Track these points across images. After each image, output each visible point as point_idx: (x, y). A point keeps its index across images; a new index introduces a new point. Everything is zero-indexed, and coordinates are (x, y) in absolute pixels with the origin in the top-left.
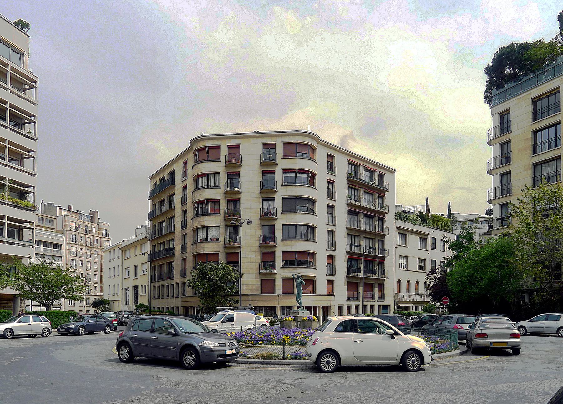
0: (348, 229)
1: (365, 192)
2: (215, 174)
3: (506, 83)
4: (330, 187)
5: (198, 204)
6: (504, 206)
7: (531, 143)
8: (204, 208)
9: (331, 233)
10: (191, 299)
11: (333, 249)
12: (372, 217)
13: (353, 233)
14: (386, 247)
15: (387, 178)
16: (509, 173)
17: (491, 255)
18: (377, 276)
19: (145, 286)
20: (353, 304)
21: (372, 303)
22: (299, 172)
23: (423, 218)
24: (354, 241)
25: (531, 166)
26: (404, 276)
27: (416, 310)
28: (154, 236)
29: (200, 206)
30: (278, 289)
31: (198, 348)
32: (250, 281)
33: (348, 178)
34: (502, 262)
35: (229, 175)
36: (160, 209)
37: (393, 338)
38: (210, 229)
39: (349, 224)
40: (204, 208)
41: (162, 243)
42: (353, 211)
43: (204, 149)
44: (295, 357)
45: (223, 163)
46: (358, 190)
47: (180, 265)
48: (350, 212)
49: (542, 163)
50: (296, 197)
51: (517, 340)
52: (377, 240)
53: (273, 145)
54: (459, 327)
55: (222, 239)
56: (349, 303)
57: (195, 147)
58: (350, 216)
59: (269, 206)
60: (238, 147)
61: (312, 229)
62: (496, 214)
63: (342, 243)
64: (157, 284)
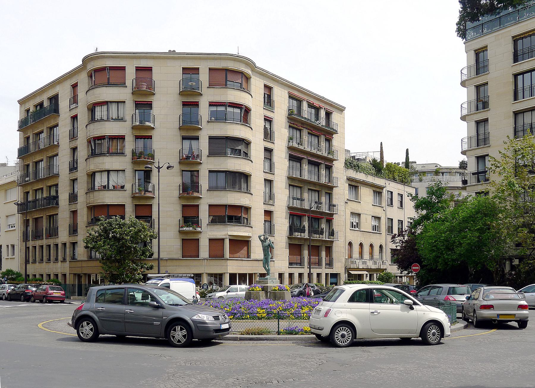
0: (290, 178)
1: (309, 133)
2: (118, 102)
3: (483, 15)
4: (268, 126)
5: (95, 141)
6: (481, 159)
7: (512, 88)
8: (99, 145)
9: (269, 182)
10: (84, 264)
11: (271, 202)
12: (317, 165)
13: (295, 183)
14: (334, 202)
15: (335, 117)
16: (486, 121)
17: (470, 217)
18: (325, 237)
19: (13, 246)
20: (296, 271)
21: (319, 271)
22: (229, 106)
23: (378, 167)
24: (297, 193)
25: (512, 114)
26: (356, 238)
27: (370, 280)
28: (27, 179)
29: (97, 142)
30: (204, 251)
31: (190, 321)
32: (167, 239)
33: (289, 115)
34: (483, 225)
35: (138, 105)
36: (36, 143)
37: (412, 308)
38: (111, 173)
39: (291, 171)
40: (99, 145)
41: (39, 189)
42: (295, 156)
43: (103, 69)
44: (291, 332)
46: (300, 130)
47: (68, 219)
48: (292, 158)
49: (523, 112)
50: (227, 137)
51: (525, 312)
52: (324, 193)
53: (196, 70)
54: (451, 299)
55: (128, 187)
56: (292, 271)
57: (91, 66)
58: (291, 162)
59: (191, 148)
60: (150, 69)
61: (246, 177)
62: (472, 167)
63: (282, 196)
64: (31, 244)
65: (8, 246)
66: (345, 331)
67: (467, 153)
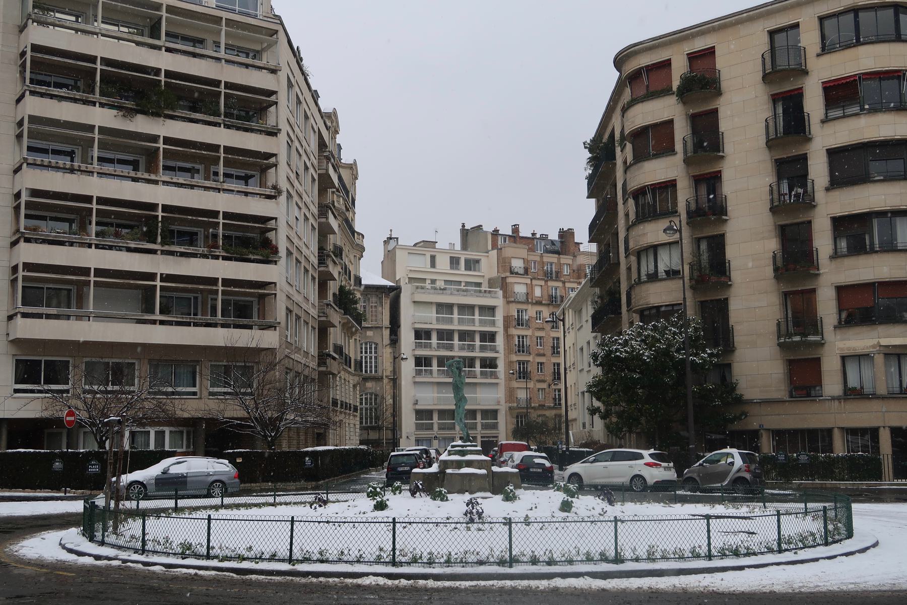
30: (832, 385)
45: (679, 157)
60: (710, 53)
66: (638, 483)
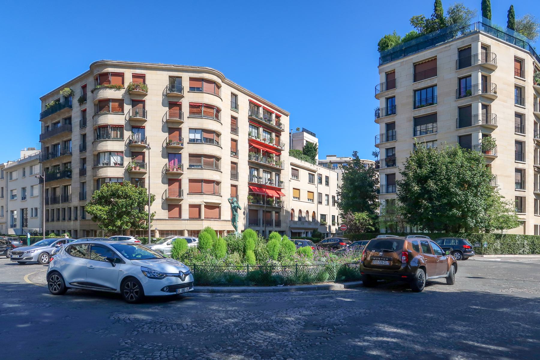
16: (394, 123)
19: (36, 209)
30: (185, 214)
57: (96, 73)
64: (51, 207)
65: (32, 209)
67: (380, 146)
